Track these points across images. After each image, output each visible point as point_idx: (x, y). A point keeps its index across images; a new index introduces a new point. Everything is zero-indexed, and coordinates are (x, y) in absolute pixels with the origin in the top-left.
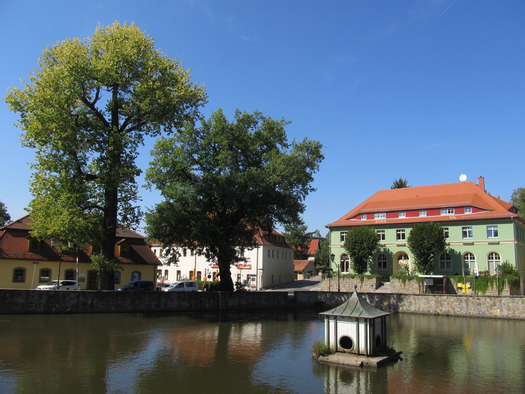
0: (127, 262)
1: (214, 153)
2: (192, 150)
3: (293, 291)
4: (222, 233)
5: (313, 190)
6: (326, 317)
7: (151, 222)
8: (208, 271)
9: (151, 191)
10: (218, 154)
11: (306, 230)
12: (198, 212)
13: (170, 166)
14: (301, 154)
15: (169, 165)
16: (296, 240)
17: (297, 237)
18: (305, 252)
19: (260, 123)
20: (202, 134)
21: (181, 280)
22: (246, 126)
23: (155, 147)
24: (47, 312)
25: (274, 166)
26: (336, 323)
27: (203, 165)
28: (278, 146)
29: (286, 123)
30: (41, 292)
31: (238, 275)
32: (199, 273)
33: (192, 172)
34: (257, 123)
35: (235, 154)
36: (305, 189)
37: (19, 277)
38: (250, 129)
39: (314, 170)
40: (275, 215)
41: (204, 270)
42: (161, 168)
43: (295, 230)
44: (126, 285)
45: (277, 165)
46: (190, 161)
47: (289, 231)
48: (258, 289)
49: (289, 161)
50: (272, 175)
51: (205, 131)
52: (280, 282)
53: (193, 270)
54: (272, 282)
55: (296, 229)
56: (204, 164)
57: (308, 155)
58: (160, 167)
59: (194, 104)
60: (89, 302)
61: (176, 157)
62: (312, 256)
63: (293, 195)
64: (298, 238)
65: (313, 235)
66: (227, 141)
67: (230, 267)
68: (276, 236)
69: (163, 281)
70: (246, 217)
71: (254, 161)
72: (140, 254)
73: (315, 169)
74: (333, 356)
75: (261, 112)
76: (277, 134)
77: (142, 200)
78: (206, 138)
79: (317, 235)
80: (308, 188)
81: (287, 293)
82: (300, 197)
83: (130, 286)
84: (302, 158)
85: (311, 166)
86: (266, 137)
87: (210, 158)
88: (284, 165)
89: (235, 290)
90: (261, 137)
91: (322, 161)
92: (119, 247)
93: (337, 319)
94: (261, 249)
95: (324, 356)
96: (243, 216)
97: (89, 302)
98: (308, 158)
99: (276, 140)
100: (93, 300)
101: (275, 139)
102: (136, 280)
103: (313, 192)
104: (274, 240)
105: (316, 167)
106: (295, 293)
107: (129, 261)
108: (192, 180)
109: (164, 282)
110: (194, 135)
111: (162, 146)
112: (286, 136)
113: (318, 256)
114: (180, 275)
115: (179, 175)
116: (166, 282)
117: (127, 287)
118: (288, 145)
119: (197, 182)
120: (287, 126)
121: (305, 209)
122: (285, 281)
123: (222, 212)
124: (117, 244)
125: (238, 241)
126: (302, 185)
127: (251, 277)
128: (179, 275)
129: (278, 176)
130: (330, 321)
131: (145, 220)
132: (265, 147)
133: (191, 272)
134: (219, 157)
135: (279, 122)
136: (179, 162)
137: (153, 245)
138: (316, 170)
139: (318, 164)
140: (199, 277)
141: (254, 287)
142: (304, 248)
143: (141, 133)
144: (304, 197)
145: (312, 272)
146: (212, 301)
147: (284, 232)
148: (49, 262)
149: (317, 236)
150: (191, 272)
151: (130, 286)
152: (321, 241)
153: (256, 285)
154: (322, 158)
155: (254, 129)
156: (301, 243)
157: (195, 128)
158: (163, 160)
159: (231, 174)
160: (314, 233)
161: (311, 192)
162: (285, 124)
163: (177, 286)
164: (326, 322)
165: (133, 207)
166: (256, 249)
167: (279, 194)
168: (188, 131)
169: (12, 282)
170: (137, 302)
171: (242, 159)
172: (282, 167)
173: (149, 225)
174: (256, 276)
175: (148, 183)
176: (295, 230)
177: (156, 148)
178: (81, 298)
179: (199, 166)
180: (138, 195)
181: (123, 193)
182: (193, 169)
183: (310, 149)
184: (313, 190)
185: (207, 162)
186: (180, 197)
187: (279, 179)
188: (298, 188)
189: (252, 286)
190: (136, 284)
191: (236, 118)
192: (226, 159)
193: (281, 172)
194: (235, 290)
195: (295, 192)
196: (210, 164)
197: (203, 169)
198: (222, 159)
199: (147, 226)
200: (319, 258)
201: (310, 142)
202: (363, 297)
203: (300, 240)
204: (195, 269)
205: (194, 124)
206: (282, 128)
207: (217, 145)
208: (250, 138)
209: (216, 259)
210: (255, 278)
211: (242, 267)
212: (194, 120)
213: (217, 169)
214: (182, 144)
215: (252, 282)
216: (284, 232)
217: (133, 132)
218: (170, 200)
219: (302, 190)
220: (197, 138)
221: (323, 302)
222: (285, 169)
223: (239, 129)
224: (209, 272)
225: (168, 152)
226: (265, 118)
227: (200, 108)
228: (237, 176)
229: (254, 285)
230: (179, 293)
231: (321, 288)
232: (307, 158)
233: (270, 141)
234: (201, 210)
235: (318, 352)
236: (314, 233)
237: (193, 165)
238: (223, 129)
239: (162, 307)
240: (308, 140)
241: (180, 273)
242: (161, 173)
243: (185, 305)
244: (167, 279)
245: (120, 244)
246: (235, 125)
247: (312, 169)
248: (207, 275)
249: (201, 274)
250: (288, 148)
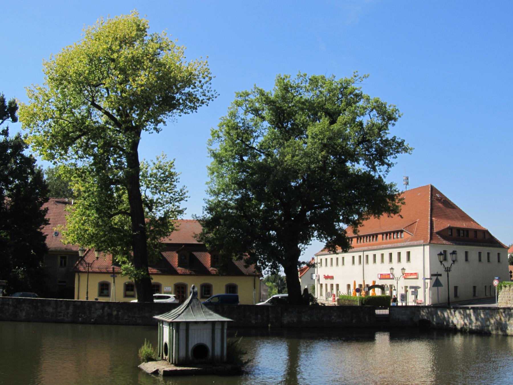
24: (73, 322)
37: (105, 292)
60: (115, 313)
97: (115, 313)
100: (118, 312)
107: (188, 271)
146: (259, 316)
148: (237, 277)
153: (423, 301)
178: (106, 309)
202: (468, 311)
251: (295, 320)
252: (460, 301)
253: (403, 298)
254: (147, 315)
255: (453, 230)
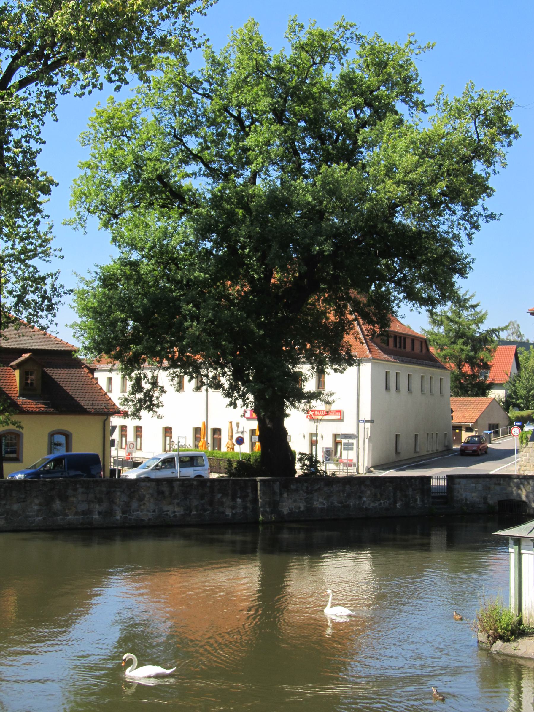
0: (37, 410)
1: (239, 131)
2: (181, 127)
3: (444, 476)
4: (262, 332)
5: (492, 216)
6: (511, 542)
7: (88, 310)
8: (238, 427)
9: (85, 233)
10: (247, 134)
11: (482, 322)
12: (201, 281)
13: (128, 170)
14: (457, 126)
15: (126, 167)
16: (458, 347)
17: (461, 341)
18: (482, 378)
19: (354, 49)
20: (206, 85)
21: (173, 451)
22: (318, 60)
23: (90, 124)
25: (388, 157)
26: (520, 554)
27: (210, 162)
28: (400, 107)
29: (420, 48)
30: (214, 480)
31: (311, 435)
32: (217, 431)
33: (186, 183)
34: (345, 51)
35: (289, 133)
36: (472, 217)
38: (326, 69)
39: (492, 167)
40: (398, 283)
41: (228, 425)
42: (110, 176)
43: (457, 323)
44: (35, 465)
45: (396, 157)
46: (177, 154)
47: (441, 325)
48: (361, 470)
49: (428, 144)
50: (383, 181)
51: (212, 78)
52: (416, 452)
53: (200, 425)
54: (397, 453)
55: (457, 319)
56: (214, 162)
57: (476, 128)
58: (107, 173)
59: (182, 10)
61: (144, 147)
62: (500, 386)
63: (439, 232)
64: (464, 344)
65: (503, 335)
66: (269, 100)
67: (287, 415)
68: (405, 339)
69: (130, 454)
70: (323, 291)
71: (338, 149)
72: (68, 390)
73: (496, 165)
74: (530, 641)
75: (353, 23)
76: (396, 78)
77: (63, 257)
78: (216, 95)
79: (513, 334)
80: (480, 214)
81: (429, 478)
82: (457, 238)
83: (45, 466)
84: (460, 136)
85: (484, 155)
86: (368, 87)
87: (229, 145)
88: (415, 154)
89: (299, 472)
90: (355, 86)
91: (514, 142)
92: (17, 373)
93: (522, 547)
94: (366, 368)
95: (508, 640)
96: (314, 289)
98: (478, 137)
99: (395, 93)
101: (392, 89)
102: (61, 452)
103: (492, 222)
104: (400, 347)
105: (497, 159)
106: (450, 478)
108: (185, 202)
109: (134, 455)
110: (186, 88)
111: (108, 121)
112: (420, 83)
113: (514, 385)
114: (171, 438)
115: (153, 191)
116: (137, 456)
117: (38, 468)
118: (426, 104)
119: (198, 206)
120: (422, 56)
121: (470, 268)
122: (428, 451)
123: (260, 279)
124: (11, 366)
125: (306, 350)
126: (463, 205)
127: (344, 441)
128: (168, 438)
129: (398, 183)
130: (522, 551)
131: (74, 305)
132: (367, 111)
133: (197, 431)
134: (250, 141)
135: (403, 47)
136: (150, 160)
137: (98, 366)
138: (498, 167)
139: (504, 150)
140: (217, 443)
141: (350, 465)
142: (479, 367)
143: (52, 89)
144: (470, 236)
145: (497, 426)
146: (239, 500)
147: (428, 327)
148: (71, 416)
149: (512, 338)
150: (197, 431)
151: (45, 466)
152: (520, 349)
153: (355, 460)
154: (512, 136)
155: (337, 64)
156: (472, 354)
157: (188, 70)
158: (111, 155)
159: (282, 183)
160: (502, 330)
161: (487, 222)
162: (417, 51)
163: (157, 465)
164: (512, 556)
165: (41, 274)
166: (355, 368)
167: (402, 230)
168: (170, 79)
169: (22, 462)
170: (57, 505)
171: (308, 144)
172: (410, 159)
173: (84, 319)
174: (356, 437)
175: (79, 214)
176: (457, 323)
177: (93, 126)
179: (201, 165)
180: (53, 245)
181: (17, 243)
182: (187, 175)
183: (482, 112)
184: (492, 216)
185: (221, 156)
186: (155, 246)
187: (402, 192)
188: (454, 213)
189: (346, 462)
190: (58, 461)
191: (290, 41)
192: (269, 145)
193: (407, 173)
194: (299, 472)
195: (443, 224)
196: (228, 159)
197: (213, 173)
198: (257, 146)
199: (79, 321)
200: (515, 392)
201: (481, 93)
203: (469, 348)
204: (206, 425)
205: (184, 62)
206: (408, 63)
207: (244, 110)
208: (327, 90)
209: (251, 397)
210: (352, 444)
211: (320, 417)
212: (185, 50)
213: (247, 173)
214: (156, 112)
215: (344, 453)
216: (428, 327)
217: (32, 87)
218: (130, 253)
219: (463, 218)
220: (195, 96)
221: (524, 502)
222: (418, 165)
223: (298, 67)
224: (240, 429)
225: (123, 136)
226: (364, 37)
227: (195, 18)
228: (295, 188)
229: (351, 460)
230: (158, 481)
231: (518, 467)
232: (475, 137)
233: (377, 97)
234: (207, 276)
235: (491, 632)
236: (502, 330)
237: (187, 163)
238: (257, 69)
239: (119, 516)
240: (477, 89)
241: (171, 433)
242: (108, 187)
243: (174, 512)
244: (141, 449)
245: (18, 366)
246: (288, 58)
247: (489, 163)
248: (235, 436)
249: (220, 434)
250: (424, 111)
251: (302, 506)
252: (401, 461)
253: (329, 456)
254: (16, 507)
255: (416, 342)
